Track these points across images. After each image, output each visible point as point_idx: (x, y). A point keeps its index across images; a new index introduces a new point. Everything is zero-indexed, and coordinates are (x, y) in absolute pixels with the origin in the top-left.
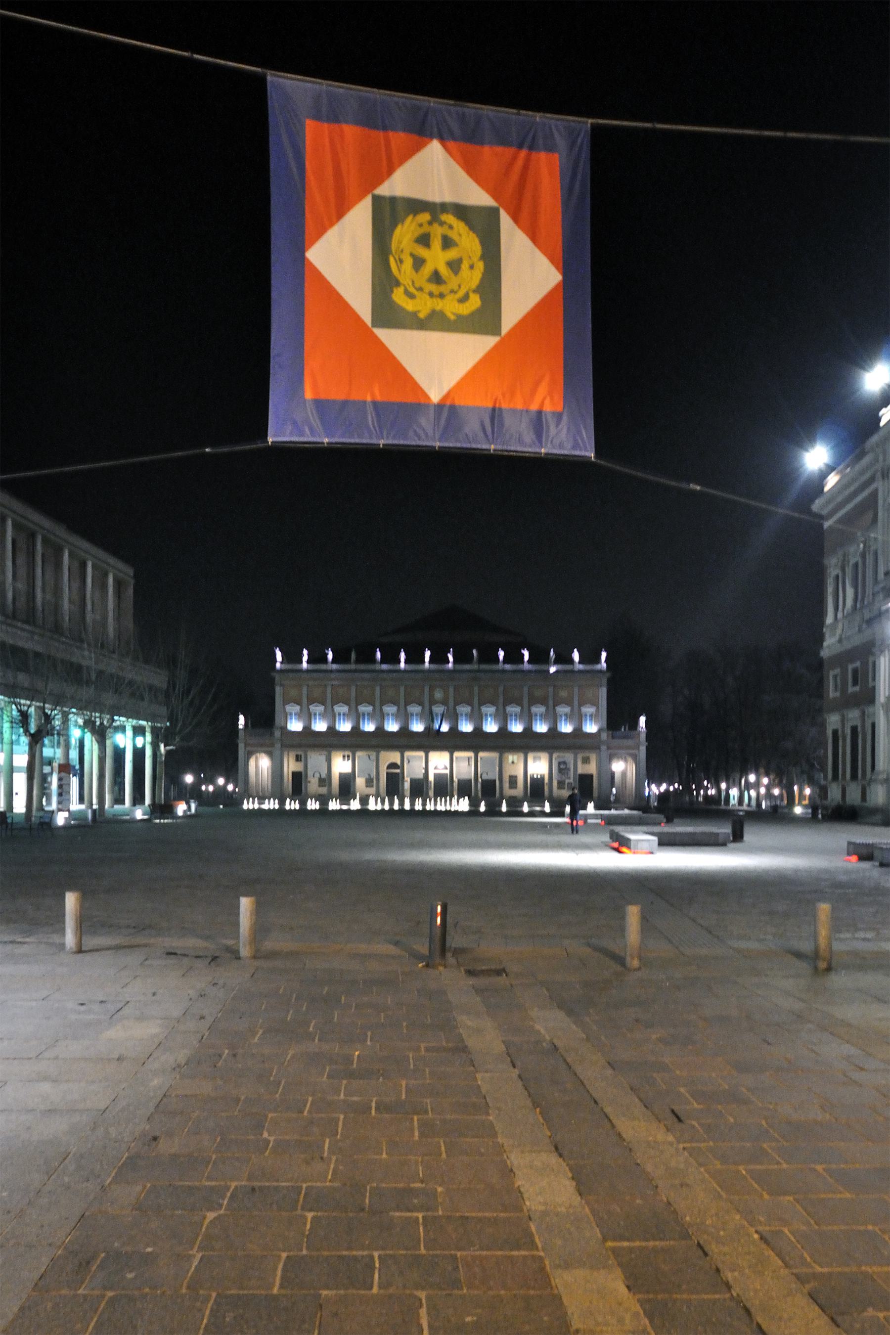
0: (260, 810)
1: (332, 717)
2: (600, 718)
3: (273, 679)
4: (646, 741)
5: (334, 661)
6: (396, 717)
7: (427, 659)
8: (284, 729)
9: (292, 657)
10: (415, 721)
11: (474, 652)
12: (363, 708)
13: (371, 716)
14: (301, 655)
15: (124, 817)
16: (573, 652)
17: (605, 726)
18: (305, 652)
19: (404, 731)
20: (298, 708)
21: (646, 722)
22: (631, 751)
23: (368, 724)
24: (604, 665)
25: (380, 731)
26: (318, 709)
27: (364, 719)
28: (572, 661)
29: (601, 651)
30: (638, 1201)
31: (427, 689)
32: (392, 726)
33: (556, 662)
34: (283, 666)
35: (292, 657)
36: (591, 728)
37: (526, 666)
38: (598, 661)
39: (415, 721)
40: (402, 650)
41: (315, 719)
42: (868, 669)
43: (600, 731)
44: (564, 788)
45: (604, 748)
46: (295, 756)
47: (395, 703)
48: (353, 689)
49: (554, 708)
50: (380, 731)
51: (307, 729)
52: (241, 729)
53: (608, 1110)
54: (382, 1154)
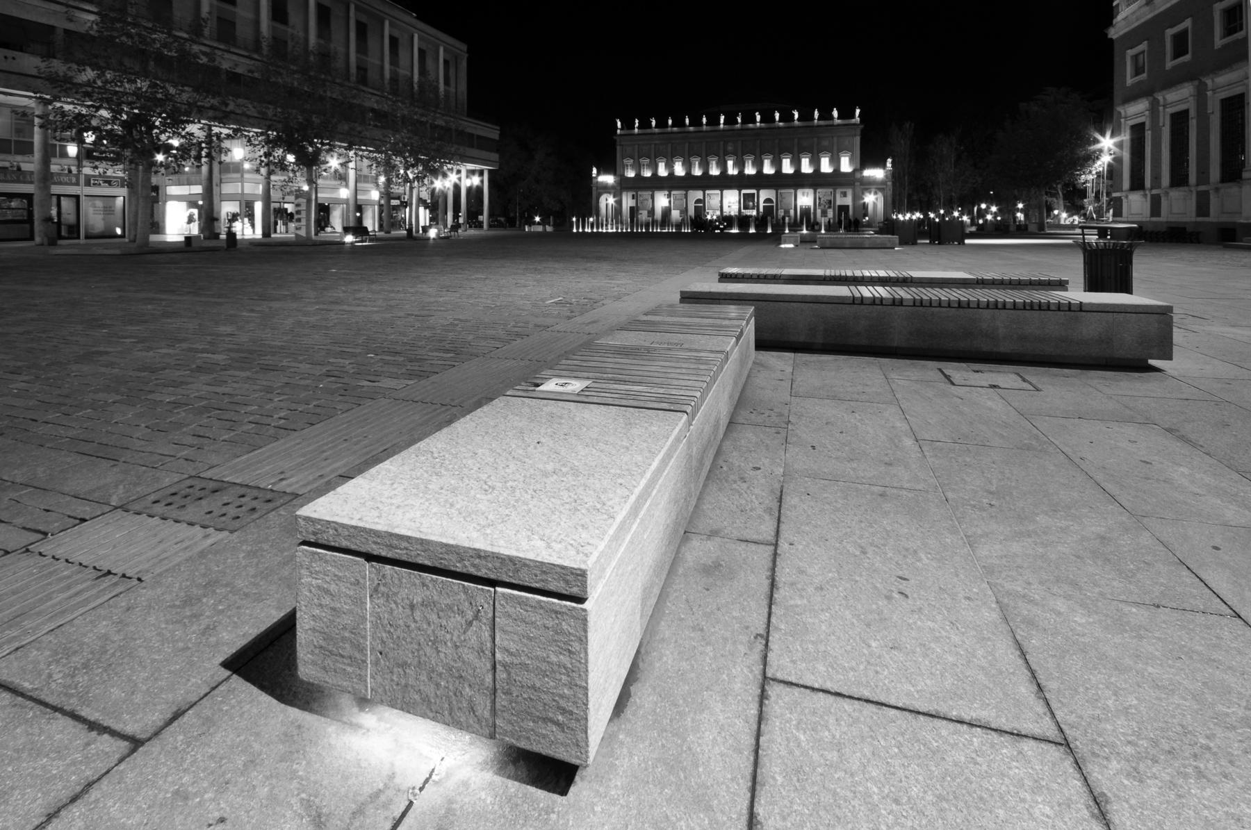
3: (615, 141)
5: (656, 127)
9: (628, 125)
14: (635, 124)
18: (637, 121)
31: (722, 143)
35: (628, 125)
37: (796, 122)
38: (853, 116)
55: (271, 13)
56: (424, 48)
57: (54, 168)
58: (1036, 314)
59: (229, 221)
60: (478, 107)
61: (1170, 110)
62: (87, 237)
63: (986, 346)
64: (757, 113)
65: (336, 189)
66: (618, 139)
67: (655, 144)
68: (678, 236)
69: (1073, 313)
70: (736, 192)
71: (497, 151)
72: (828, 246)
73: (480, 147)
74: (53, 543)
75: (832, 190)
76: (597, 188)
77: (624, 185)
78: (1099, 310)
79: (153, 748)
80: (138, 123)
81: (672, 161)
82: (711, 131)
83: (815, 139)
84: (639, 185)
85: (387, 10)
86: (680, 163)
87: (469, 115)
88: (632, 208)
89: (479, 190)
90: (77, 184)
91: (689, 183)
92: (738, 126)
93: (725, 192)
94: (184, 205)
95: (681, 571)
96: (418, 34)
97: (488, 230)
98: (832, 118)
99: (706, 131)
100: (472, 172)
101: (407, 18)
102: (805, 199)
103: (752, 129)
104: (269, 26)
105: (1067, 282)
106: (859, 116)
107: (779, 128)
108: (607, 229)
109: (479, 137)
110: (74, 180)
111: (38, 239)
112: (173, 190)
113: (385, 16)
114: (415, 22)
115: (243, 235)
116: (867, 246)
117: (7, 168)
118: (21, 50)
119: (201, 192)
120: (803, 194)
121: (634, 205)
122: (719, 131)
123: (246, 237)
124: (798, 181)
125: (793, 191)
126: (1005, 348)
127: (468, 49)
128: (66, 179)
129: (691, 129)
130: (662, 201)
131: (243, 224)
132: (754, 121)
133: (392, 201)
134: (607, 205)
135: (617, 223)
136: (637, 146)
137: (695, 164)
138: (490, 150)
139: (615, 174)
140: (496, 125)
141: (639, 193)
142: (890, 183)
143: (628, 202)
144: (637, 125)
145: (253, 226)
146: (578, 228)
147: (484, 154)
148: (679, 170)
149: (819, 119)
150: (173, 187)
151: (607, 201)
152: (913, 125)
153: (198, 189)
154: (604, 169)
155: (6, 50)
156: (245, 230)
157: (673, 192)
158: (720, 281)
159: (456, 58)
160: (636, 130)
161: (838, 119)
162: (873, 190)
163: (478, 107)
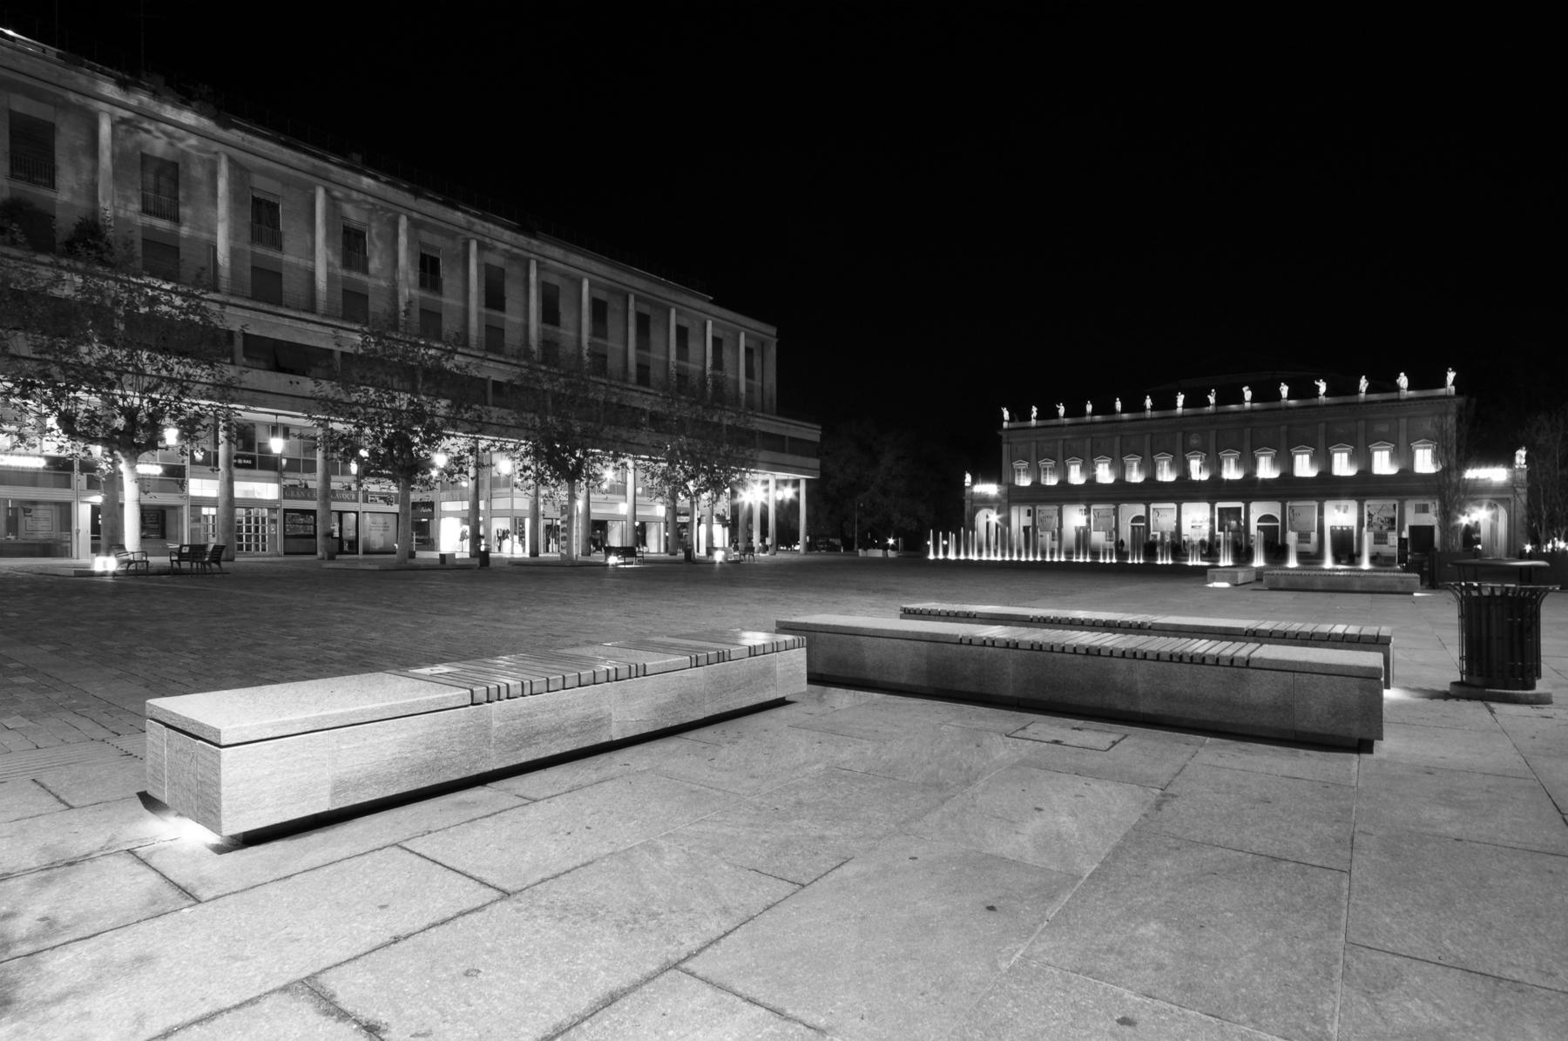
5: (1065, 416)
9: (1021, 414)
14: (1031, 412)
18: (1034, 409)
19: (1151, 481)
20: (1052, 463)
21: (1455, 378)
24: (1450, 388)
29: (1447, 370)
31: (1179, 435)
34: (1154, 413)
35: (1021, 414)
37: (1322, 399)
38: (1443, 384)
49: (1327, 448)
56: (721, 336)
57: (335, 485)
58: (1186, 668)
59: (499, 538)
60: (790, 401)
62: (365, 552)
63: (1121, 704)
64: (1245, 389)
65: (615, 503)
66: (1004, 436)
67: (1064, 440)
68: (1095, 569)
69: (1236, 670)
70: (1205, 506)
71: (818, 456)
72: (1281, 586)
73: (793, 452)
75: (1396, 502)
76: (972, 501)
77: (1014, 497)
78: (1274, 667)
79: (75, 811)
80: (400, 441)
81: (1093, 462)
82: (1192, 416)
83: (1362, 424)
84: (1037, 496)
85: (673, 297)
86: (1107, 466)
87: (779, 414)
88: (1026, 529)
89: (794, 505)
90: (357, 501)
91: (1121, 492)
92: (1210, 408)
93: (1186, 506)
94: (458, 521)
96: (710, 320)
97: (806, 554)
99: (1152, 419)
100: (785, 482)
101: (698, 303)
102: (1340, 516)
103: (1235, 412)
104: (538, 329)
106: (1454, 383)
107: (1289, 408)
108: (988, 555)
109: (792, 439)
110: (353, 497)
111: (320, 554)
112: (447, 506)
113: (672, 304)
114: (707, 306)
115: (512, 553)
116: (1358, 588)
117: (296, 486)
118: (304, 375)
120: (1338, 507)
122: (1176, 417)
123: (516, 556)
124: (1327, 488)
125: (1315, 504)
126: (1145, 707)
127: (777, 333)
128: (346, 496)
129: (1125, 416)
130: (1075, 518)
131: (513, 543)
132: (1241, 400)
134: (988, 524)
135: (1003, 548)
136: (1034, 444)
137: (1132, 466)
138: (808, 455)
139: (999, 482)
140: (817, 423)
141: (1038, 508)
142: (1523, 491)
143: (1019, 519)
144: (1034, 414)
145: (523, 545)
146: (936, 552)
147: (799, 460)
148: (1105, 475)
149: (1368, 391)
150: (448, 503)
151: (988, 519)
152: (1474, 400)
153: (466, 505)
154: (982, 475)
155: (291, 376)
156: (515, 548)
157: (1094, 507)
158: (902, 617)
159: (763, 344)
160: (1033, 422)
161: (1409, 389)
162: (1486, 502)
163: (790, 401)
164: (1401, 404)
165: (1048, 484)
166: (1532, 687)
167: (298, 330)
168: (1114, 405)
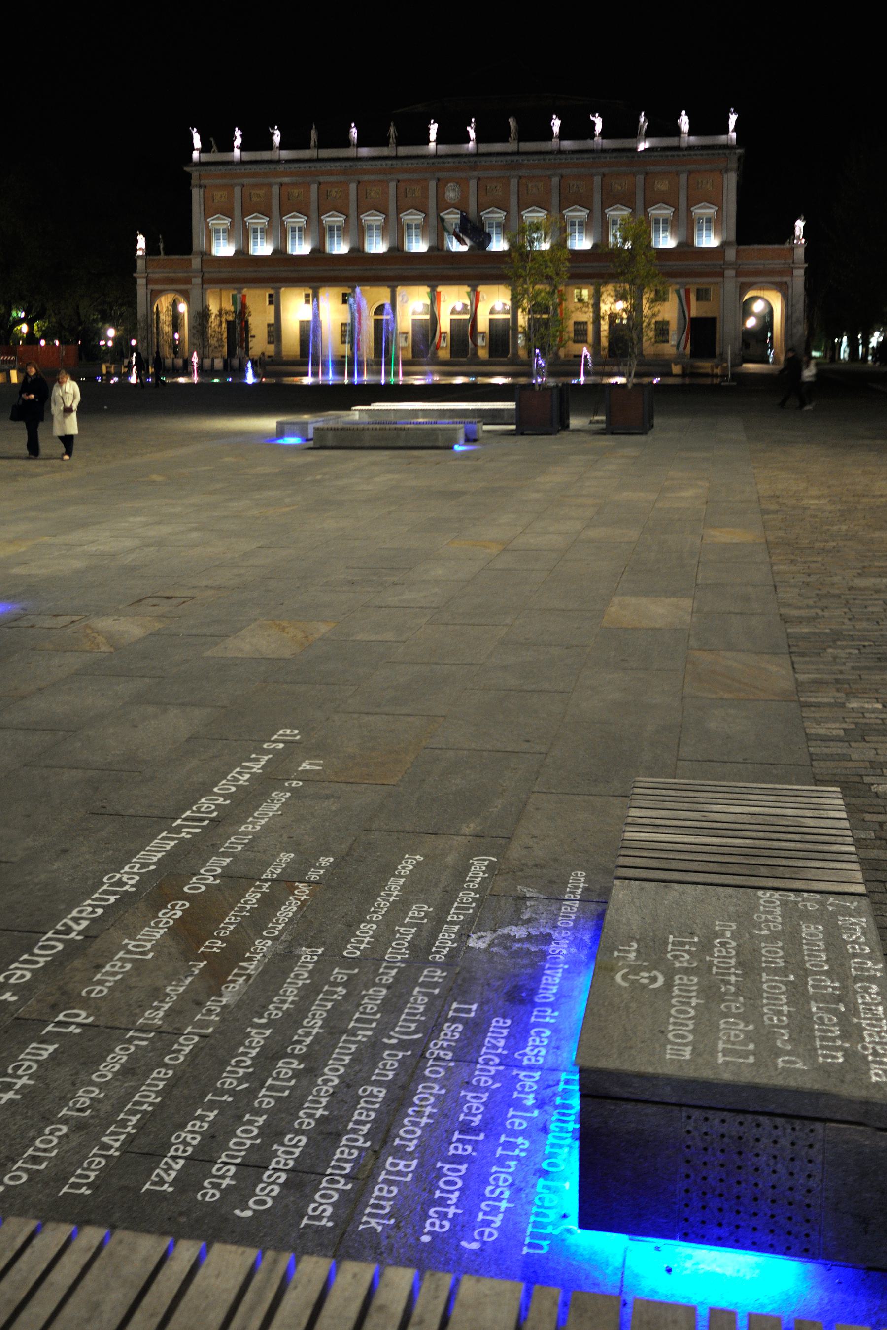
0: (351, 386)
1: (282, 235)
2: (725, 226)
3: (189, 176)
4: (806, 261)
6: (384, 230)
7: (433, 136)
8: (206, 255)
10: (577, 234)
11: (512, 121)
12: (327, 219)
13: (343, 231)
15: (15, 571)
16: (680, 115)
17: (733, 237)
18: (238, 133)
20: (381, 218)
21: (737, 121)
22: (777, 279)
23: (338, 244)
25: (357, 254)
26: (374, 219)
27: (332, 237)
28: (677, 132)
30: (111, 332)
31: (433, 184)
32: (377, 246)
33: (649, 135)
36: (709, 241)
37: (598, 142)
39: (577, 234)
40: (683, 113)
41: (255, 238)
42: (473, 411)
43: (724, 245)
44: (159, 254)
45: (729, 273)
46: (341, 295)
47: (381, 209)
48: (314, 188)
49: (358, 217)
50: (357, 254)
51: (242, 254)
52: (139, 256)
53: (131, 811)
54: (579, 376)
55: (263, 285)
61: (573, 1222)
66: (195, 173)
74: (798, 822)
95: (756, 1117)
98: (676, 131)
105: (708, 300)
106: (735, 130)
119: (514, 407)
121: (309, 317)
133: (516, 180)
136: (237, 190)
138: (388, 187)
144: (238, 142)
160: (237, 153)
164: (681, 153)
165: (335, 252)
166: (278, 423)
167: (252, 1309)
168: (348, 132)
